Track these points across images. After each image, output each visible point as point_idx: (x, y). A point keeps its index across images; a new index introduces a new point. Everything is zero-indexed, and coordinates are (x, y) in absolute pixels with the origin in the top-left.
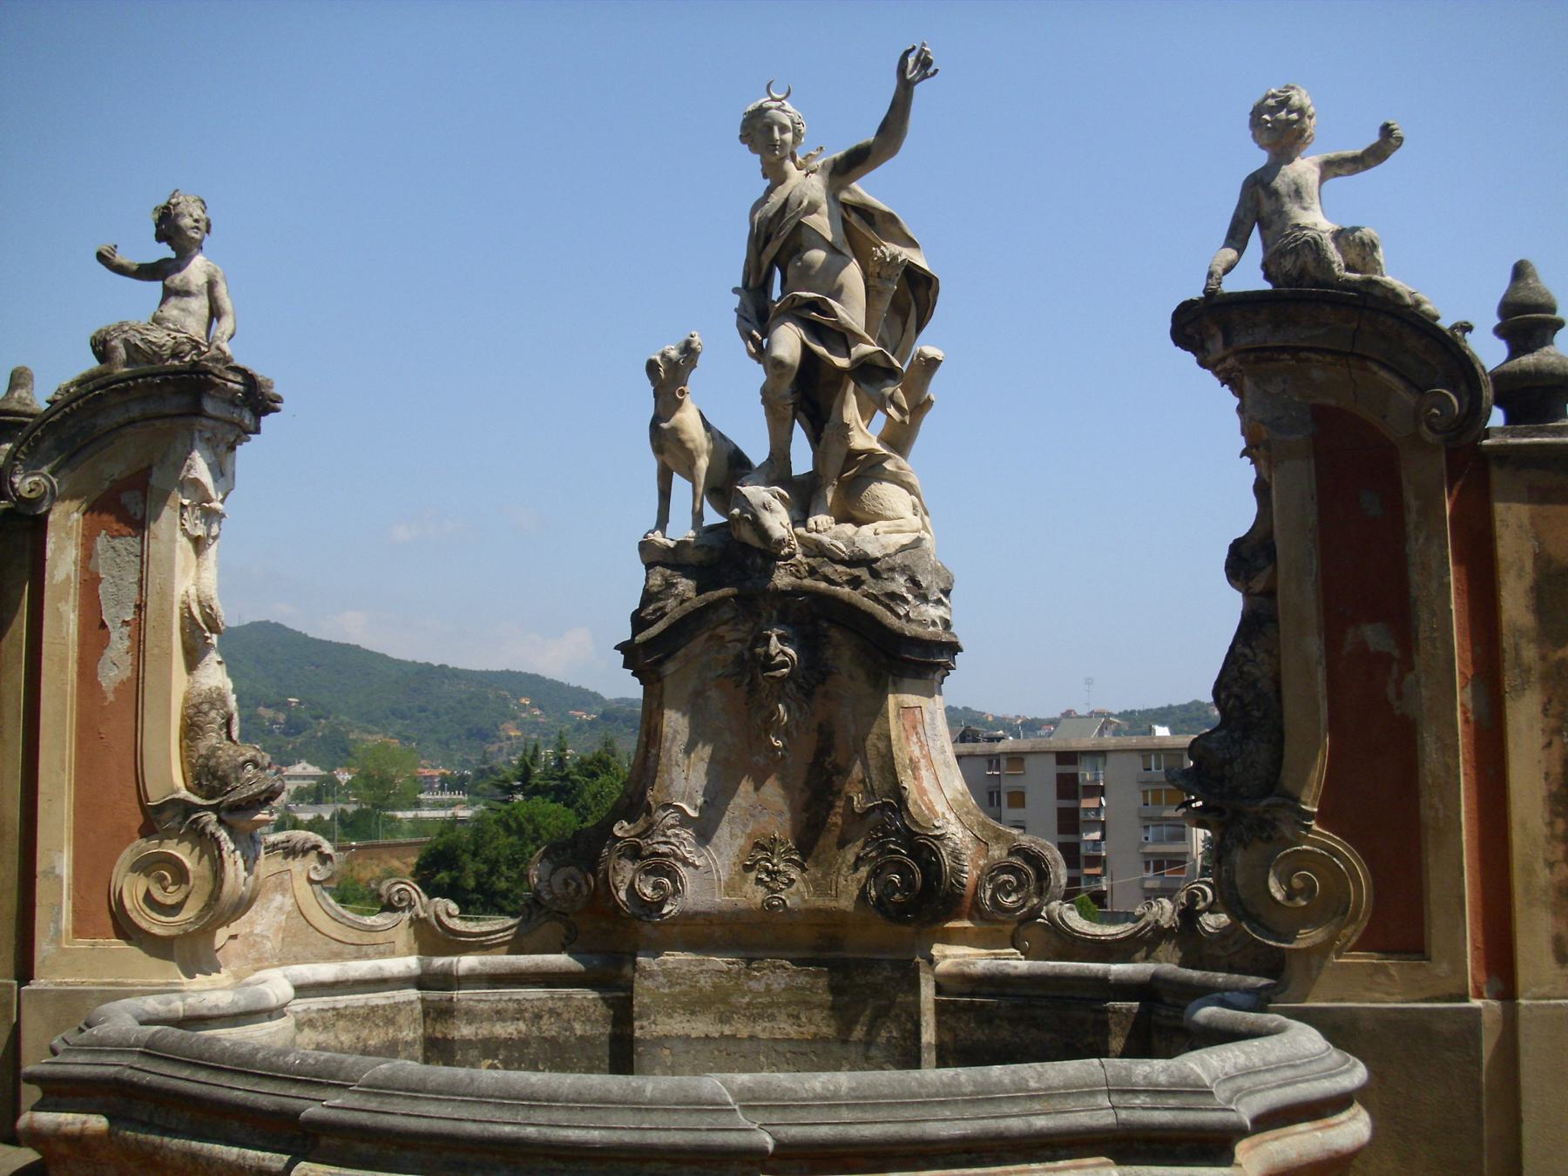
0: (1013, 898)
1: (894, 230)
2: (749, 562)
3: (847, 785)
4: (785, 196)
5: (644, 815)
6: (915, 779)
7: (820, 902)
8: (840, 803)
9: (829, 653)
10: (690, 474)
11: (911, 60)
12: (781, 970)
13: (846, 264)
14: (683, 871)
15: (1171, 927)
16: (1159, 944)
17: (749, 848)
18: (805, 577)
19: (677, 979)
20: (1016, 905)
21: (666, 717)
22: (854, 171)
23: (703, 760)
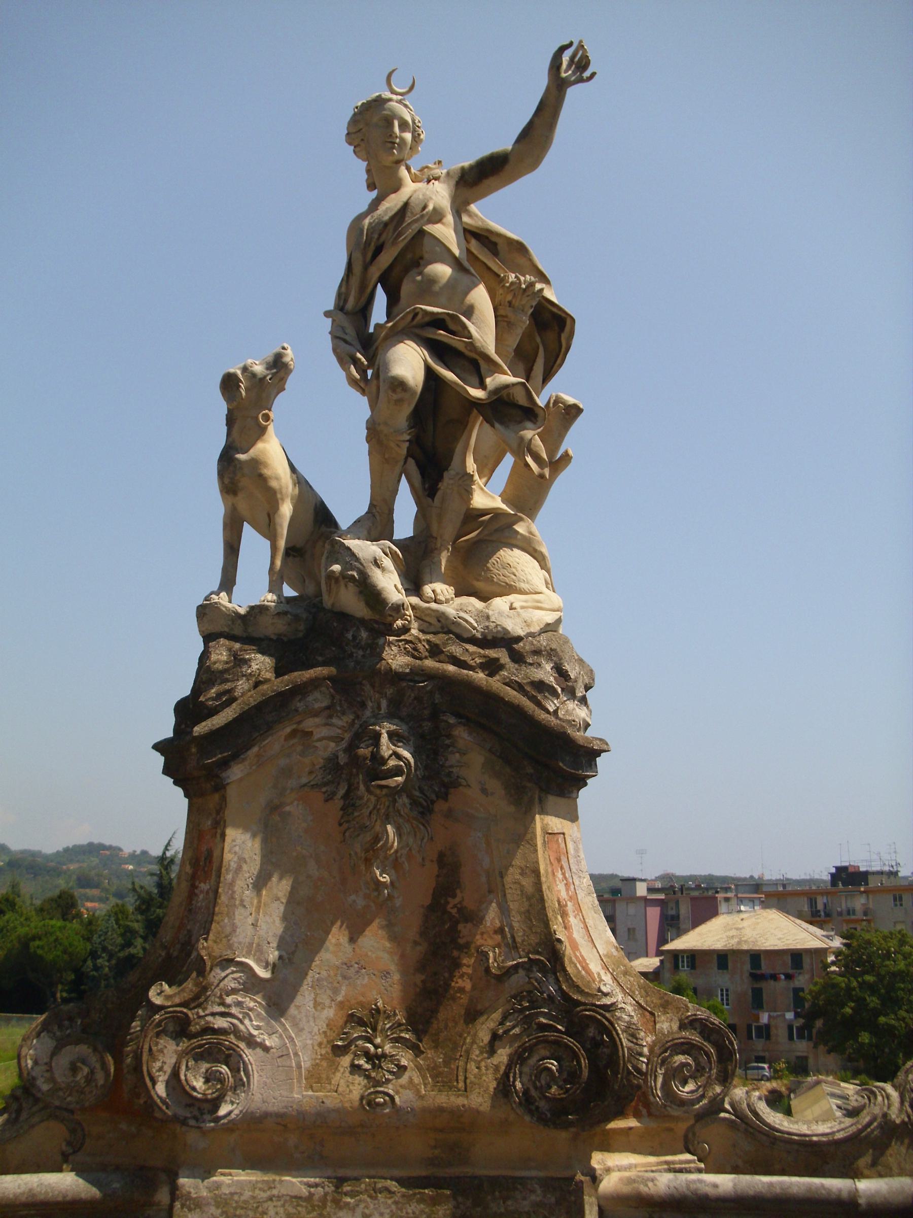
0: (690, 1087)
1: (522, 261)
2: (349, 636)
3: (478, 937)
4: (405, 199)
5: (194, 975)
6: (565, 928)
7: (443, 1099)
8: (468, 962)
9: (454, 758)
10: (268, 530)
11: (566, 58)
12: (385, 1194)
13: (476, 285)
14: (250, 1056)
15: (903, 1122)
16: (887, 1146)
17: (341, 1022)
18: (426, 658)
19: (236, 1209)
20: (694, 1096)
21: (228, 839)
22: (486, 182)
23: (278, 899)
